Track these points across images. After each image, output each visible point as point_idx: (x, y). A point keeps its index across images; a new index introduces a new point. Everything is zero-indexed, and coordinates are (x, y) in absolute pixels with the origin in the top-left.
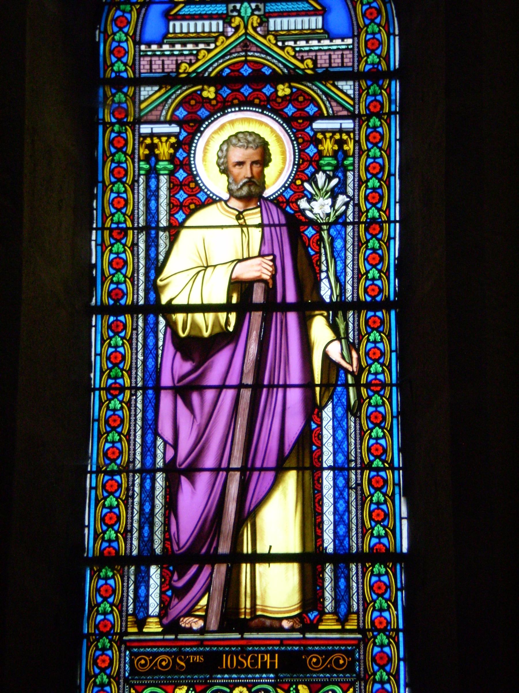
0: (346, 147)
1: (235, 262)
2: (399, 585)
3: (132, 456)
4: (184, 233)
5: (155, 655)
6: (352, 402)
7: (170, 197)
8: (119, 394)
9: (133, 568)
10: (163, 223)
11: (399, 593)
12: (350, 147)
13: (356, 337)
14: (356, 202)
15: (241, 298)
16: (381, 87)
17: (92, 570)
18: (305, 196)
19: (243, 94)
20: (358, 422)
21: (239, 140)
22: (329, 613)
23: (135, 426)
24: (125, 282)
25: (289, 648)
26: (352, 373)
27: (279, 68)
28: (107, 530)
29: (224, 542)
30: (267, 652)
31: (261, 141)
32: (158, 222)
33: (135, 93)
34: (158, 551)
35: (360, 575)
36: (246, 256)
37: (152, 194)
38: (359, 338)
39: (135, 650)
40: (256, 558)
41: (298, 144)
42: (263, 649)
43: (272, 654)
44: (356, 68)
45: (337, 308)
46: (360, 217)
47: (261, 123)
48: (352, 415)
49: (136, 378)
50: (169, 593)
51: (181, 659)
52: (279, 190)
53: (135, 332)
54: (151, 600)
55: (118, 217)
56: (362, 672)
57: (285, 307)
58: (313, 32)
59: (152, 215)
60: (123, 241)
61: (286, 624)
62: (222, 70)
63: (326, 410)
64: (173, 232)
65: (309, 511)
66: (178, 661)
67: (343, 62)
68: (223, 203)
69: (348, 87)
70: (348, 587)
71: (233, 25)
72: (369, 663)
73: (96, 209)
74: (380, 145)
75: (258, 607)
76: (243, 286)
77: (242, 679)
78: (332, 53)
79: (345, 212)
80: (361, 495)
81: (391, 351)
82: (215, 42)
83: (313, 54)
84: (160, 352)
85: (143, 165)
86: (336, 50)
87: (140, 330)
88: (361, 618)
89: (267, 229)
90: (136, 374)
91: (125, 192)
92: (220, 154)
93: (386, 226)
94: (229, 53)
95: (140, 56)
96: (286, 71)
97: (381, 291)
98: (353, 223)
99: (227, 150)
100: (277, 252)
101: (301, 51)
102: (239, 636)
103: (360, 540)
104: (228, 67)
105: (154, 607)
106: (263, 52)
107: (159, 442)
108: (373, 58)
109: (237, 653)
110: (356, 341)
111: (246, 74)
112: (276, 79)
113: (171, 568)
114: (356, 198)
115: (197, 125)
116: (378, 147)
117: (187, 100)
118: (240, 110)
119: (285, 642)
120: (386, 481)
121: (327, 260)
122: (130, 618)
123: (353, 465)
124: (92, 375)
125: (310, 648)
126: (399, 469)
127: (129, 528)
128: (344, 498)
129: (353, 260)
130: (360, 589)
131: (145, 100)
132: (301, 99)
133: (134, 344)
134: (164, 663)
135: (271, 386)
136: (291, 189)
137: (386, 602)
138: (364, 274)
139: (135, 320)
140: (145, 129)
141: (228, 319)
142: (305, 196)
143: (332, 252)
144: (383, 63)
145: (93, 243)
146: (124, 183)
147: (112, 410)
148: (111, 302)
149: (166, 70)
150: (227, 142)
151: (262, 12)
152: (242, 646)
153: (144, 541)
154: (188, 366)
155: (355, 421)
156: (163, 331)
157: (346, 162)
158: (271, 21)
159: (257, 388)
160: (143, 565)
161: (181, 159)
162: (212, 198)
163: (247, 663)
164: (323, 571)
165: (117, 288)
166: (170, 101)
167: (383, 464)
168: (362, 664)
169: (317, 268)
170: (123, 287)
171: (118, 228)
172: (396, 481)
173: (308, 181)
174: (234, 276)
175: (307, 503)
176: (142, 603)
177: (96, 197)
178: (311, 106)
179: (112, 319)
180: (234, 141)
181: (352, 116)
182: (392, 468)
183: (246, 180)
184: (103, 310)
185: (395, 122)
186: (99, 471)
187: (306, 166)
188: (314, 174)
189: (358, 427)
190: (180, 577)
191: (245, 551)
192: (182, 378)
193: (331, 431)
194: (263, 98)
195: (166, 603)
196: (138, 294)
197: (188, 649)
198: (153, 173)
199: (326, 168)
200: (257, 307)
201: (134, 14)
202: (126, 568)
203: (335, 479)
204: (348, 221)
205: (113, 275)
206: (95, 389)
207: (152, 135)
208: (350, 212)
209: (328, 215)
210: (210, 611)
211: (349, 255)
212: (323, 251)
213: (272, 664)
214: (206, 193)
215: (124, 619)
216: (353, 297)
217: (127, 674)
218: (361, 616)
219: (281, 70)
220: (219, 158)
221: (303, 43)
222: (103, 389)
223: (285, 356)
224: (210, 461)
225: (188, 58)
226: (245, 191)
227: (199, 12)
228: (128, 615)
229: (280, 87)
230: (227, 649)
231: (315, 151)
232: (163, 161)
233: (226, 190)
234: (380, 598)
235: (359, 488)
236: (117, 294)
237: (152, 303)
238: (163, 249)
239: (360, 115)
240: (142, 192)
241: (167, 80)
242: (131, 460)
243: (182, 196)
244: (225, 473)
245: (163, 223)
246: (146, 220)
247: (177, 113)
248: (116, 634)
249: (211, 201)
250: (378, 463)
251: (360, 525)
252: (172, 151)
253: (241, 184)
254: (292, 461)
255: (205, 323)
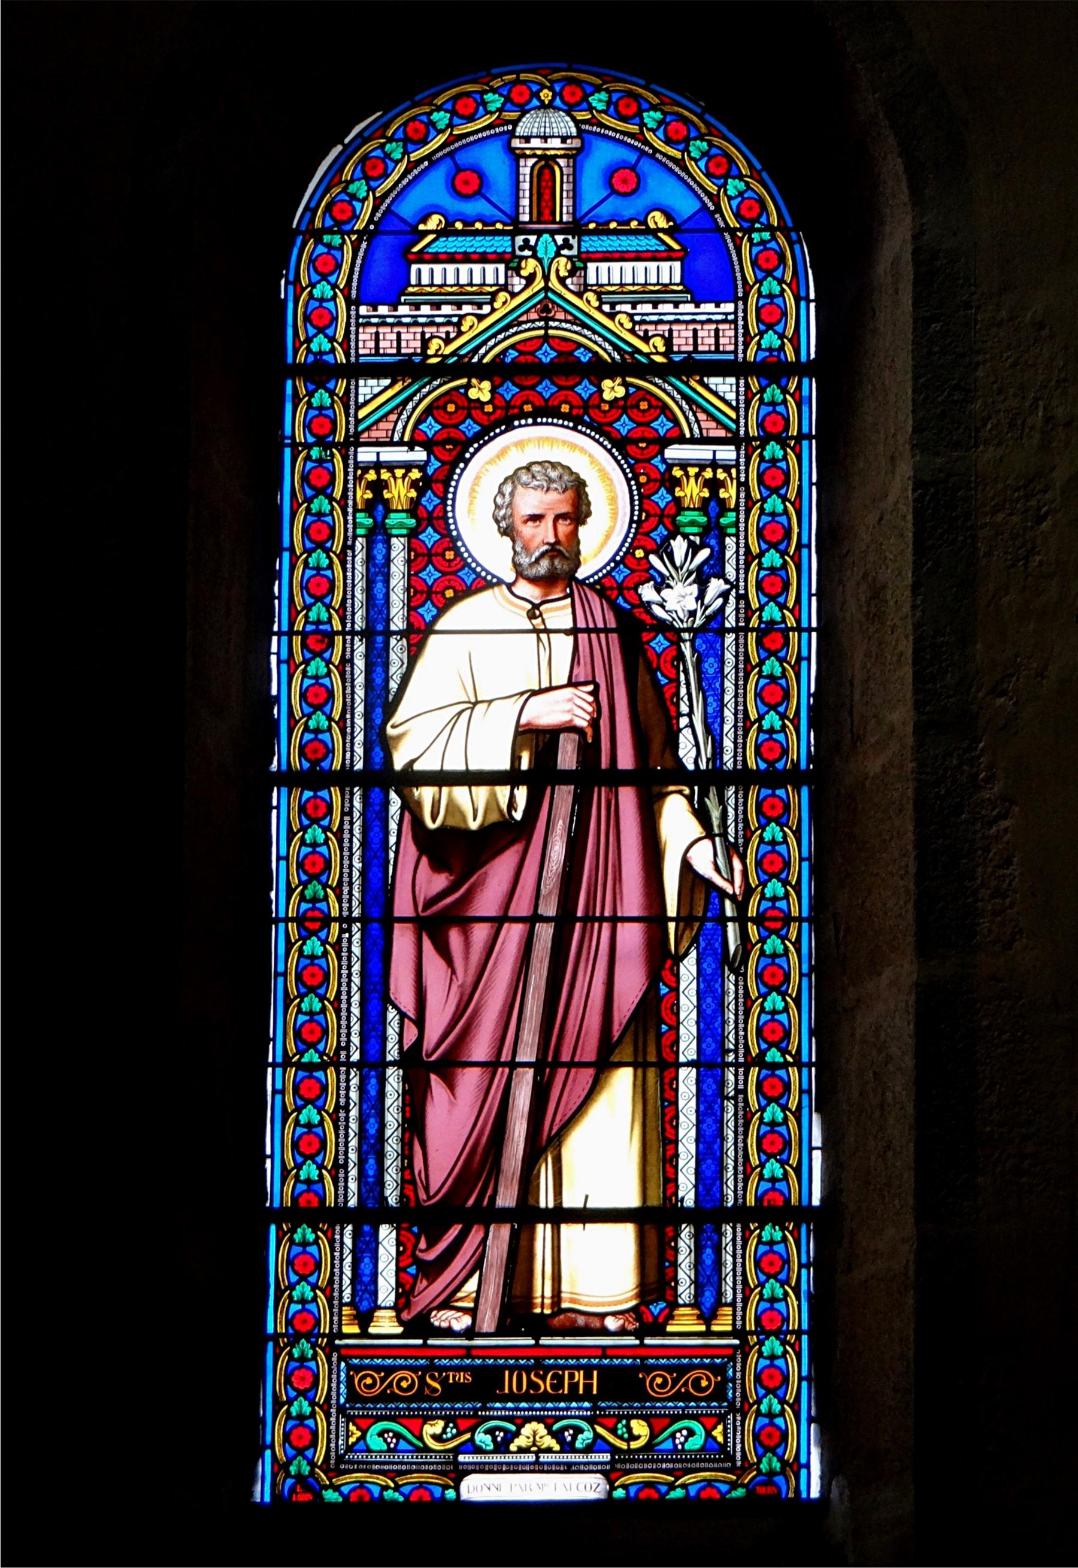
0: (723, 494)
1: (526, 696)
2: (804, 1260)
3: (343, 1039)
4: (433, 640)
5: (390, 1370)
6: (732, 948)
7: (409, 575)
8: (321, 929)
9: (350, 1227)
10: (398, 623)
11: (804, 1272)
12: (729, 493)
13: (741, 833)
14: (742, 592)
15: (535, 759)
16: (784, 391)
17: (279, 1228)
18: (652, 578)
19: (541, 394)
20: (741, 983)
21: (534, 477)
22: (685, 1305)
23: (349, 986)
24: (330, 728)
25: (616, 1362)
26: (733, 898)
27: (605, 350)
28: (304, 1163)
29: (506, 1188)
30: (578, 1368)
31: (573, 477)
32: (388, 620)
33: (347, 390)
34: (392, 1201)
35: (739, 1242)
36: (545, 684)
37: (378, 571)
38: (744, 836)
39: (356, 1361)
40: (560, 1216)
41: (639, 485)
42: (572, 1362)
43: (588, 1371)
44: (741, 355)
45: (706, 782)
46: (748, 620)
47: (573, 446)
48: (732, 970)
49: (350, 901)
50: (412, 1270)
51: (433, 1378)
52: (604, 567)
53: (347, 818)
54: (381, 1281)
55: (318, 612)
56: (738, 1400)
57: (616, 778)
58: (665, 289)
59: (377, 607)
60: (327, 655)
61: (611, 1323)
62: (504, 352)
63: (685, 961)
64: (415, 638)
65: (653, 1136)
66: (429, 1380)
67: (717, 344)
68: (504, 587)
69: (727, 388)
70: (718, 1263)
71: (524, 273)
72: (750, 1384)
73: (279, 598)
74: (783, 492)
75: (563, 1295)
76: (541, 738)
77: (536, 1410)
78: (699, 327)
79: (722, 609)
80: (744, 1108)
81: (801, 860)
82: (491, 302)
83: (667, 327)
84: (392, 855)
85: (361, 517)
86: (705, 326)
87: (356, 814)
88: (739, 1313)
89: (583, 637)
90: (350, 893)
91: (330, 566)
92: (499, 500)
93: (793, 636)
94: (517, 323)
95: (358, 325)
96: (617, 357)
97: (785, 751)
98: (735, 630)
99: (512, 494)
100: (601, 679)
101: (643, 322)
102: (533, 1342)
103: (740, 1185)
104: (512, 347)
105: (386, 1292)
106: (576, 321)
107: (391, 1014)
108: (770, 339)
109: (528, 1369)
110: (741, 841)
111: (546, 360)
112: (599, 370)
113: (415, 1229)
114: (742, 584)
115: (458, 449)
116: (779, 496)
117: (441, 403)
118: (535, 424)
119: (609, 1352)
120: (787, 1086)
121: (689, 694)
122: (346, 1311)
123: (731, 1058)
124: (273, 895)
125: (652, 1361)
126: (809, 1065)
127: (341, 1162)
128: (715, 1114)
129: (736, 696)
130: (739, 1265)
131: (366, 403)
132: (644, 406)
133: (346, 841)
134: (404, 1384)
135: (589, 919)
136: (626, 566)
137: (782, 1286)
138: (756, 721)
139: (347, 796)
140: (366, 455)
141: (512, 796)
142: (652, 578)
143: (699, 681)
144: (789, 348)
145: (274, 659)
146: (327, 551)
147: (308, 957)
148: (306, 765)
149: (403, 351)
150: (513, 478)
151: (574, 252)
152: (536, 1359)
153: (367, 1183)
154: (441, 881)
155: (737, 981)
156: (397, 817)
157: (723, 521)
158: (592, 266)
159: (564, 921)
160: (367, 1224)
161: (430, 508)
162: (485, 578)
163: (546, 1385)
164: (677, 1236)
165: (316, 739)
166: (410, 406)
167: (783, 1056)
168: (738, 1387)
169: (672, 709)
170: (325, 737)
171: (317, 632)
172: (805, 1086)
173: (656, 552)
174: (523, 721)
175: (651, 1124)
176: (365, 1284)
177: (279, 575)
178: (662, 418)
179: (308, 794)
180: (525, 477)
181: (734, 439)
182: (798, 1063)
183: (546, 547)
184: (290, 779)
185: (810, 450)
186: (286, 1063)
187: (653, 525)
188: (667, 539)
189: (741, 992)
190: (431, 1245)
191: (542, 1205)
192: (430, 902)
193: (694, 1000)
194: (577, 402)
195: (408, 1287)
196: (352, 751)
197: (444, 1362)
198: (379, 534)
199: (688, 530)
200: (566, 777)
201: (348, 249)
202: (338, 1228)
203: (699, 1082)
204: (727, 625)
205: (309, 716)
206: (277, 920)
207: (378, 465)
208: (730, 609)
209: (692, 614)
210: (482, 1300)
211: (729, 686)
212: (682, 677)
213: (588, 1387)
214: (474, 570)
215: (336, 1310)
216: (735, 762)
217: (342, 1400)
218: (739, 1309)
219: (609, 354)
220: (497, 507)
221: (647, 308)
222: (292, 920)
223: (614, 866)
224: (480, 1049)
225: (443, 329)
226: (544, 566)
227: (462, 250)
228: (342, 1305)
229: (607, 384)
230: (512, 1362)
231: (669, 498)
232: (397, 511)
233: (510, 565)
234: (772, 1281)
235: (741, 1097)
236: (316, 749)
237: (377, 767)
238: (396, 670)
239: (748, 439)
240: (360, 568)
241: (406, 369)
242: (343, 1044)
243: (431, 575)
244: (507, 1070)
245: (398, 623)
246: (368, 618)
247: (423, 427)
248: (324, 1335)
249: (484, 583)
250: (773, 1055)
251: (740, 1160)
252: (413, 494)
253: (537, 554)
254: (626, 1052)
255: (472, 806)
